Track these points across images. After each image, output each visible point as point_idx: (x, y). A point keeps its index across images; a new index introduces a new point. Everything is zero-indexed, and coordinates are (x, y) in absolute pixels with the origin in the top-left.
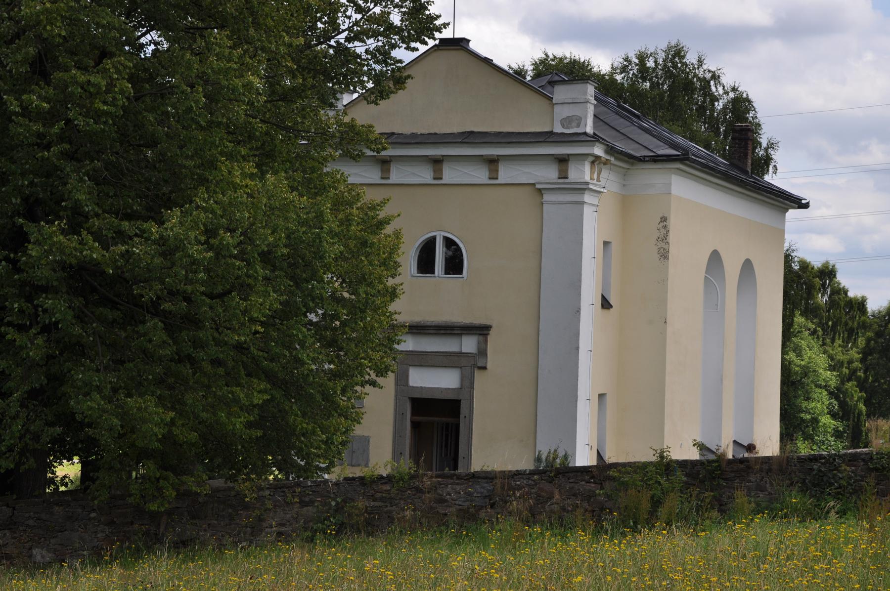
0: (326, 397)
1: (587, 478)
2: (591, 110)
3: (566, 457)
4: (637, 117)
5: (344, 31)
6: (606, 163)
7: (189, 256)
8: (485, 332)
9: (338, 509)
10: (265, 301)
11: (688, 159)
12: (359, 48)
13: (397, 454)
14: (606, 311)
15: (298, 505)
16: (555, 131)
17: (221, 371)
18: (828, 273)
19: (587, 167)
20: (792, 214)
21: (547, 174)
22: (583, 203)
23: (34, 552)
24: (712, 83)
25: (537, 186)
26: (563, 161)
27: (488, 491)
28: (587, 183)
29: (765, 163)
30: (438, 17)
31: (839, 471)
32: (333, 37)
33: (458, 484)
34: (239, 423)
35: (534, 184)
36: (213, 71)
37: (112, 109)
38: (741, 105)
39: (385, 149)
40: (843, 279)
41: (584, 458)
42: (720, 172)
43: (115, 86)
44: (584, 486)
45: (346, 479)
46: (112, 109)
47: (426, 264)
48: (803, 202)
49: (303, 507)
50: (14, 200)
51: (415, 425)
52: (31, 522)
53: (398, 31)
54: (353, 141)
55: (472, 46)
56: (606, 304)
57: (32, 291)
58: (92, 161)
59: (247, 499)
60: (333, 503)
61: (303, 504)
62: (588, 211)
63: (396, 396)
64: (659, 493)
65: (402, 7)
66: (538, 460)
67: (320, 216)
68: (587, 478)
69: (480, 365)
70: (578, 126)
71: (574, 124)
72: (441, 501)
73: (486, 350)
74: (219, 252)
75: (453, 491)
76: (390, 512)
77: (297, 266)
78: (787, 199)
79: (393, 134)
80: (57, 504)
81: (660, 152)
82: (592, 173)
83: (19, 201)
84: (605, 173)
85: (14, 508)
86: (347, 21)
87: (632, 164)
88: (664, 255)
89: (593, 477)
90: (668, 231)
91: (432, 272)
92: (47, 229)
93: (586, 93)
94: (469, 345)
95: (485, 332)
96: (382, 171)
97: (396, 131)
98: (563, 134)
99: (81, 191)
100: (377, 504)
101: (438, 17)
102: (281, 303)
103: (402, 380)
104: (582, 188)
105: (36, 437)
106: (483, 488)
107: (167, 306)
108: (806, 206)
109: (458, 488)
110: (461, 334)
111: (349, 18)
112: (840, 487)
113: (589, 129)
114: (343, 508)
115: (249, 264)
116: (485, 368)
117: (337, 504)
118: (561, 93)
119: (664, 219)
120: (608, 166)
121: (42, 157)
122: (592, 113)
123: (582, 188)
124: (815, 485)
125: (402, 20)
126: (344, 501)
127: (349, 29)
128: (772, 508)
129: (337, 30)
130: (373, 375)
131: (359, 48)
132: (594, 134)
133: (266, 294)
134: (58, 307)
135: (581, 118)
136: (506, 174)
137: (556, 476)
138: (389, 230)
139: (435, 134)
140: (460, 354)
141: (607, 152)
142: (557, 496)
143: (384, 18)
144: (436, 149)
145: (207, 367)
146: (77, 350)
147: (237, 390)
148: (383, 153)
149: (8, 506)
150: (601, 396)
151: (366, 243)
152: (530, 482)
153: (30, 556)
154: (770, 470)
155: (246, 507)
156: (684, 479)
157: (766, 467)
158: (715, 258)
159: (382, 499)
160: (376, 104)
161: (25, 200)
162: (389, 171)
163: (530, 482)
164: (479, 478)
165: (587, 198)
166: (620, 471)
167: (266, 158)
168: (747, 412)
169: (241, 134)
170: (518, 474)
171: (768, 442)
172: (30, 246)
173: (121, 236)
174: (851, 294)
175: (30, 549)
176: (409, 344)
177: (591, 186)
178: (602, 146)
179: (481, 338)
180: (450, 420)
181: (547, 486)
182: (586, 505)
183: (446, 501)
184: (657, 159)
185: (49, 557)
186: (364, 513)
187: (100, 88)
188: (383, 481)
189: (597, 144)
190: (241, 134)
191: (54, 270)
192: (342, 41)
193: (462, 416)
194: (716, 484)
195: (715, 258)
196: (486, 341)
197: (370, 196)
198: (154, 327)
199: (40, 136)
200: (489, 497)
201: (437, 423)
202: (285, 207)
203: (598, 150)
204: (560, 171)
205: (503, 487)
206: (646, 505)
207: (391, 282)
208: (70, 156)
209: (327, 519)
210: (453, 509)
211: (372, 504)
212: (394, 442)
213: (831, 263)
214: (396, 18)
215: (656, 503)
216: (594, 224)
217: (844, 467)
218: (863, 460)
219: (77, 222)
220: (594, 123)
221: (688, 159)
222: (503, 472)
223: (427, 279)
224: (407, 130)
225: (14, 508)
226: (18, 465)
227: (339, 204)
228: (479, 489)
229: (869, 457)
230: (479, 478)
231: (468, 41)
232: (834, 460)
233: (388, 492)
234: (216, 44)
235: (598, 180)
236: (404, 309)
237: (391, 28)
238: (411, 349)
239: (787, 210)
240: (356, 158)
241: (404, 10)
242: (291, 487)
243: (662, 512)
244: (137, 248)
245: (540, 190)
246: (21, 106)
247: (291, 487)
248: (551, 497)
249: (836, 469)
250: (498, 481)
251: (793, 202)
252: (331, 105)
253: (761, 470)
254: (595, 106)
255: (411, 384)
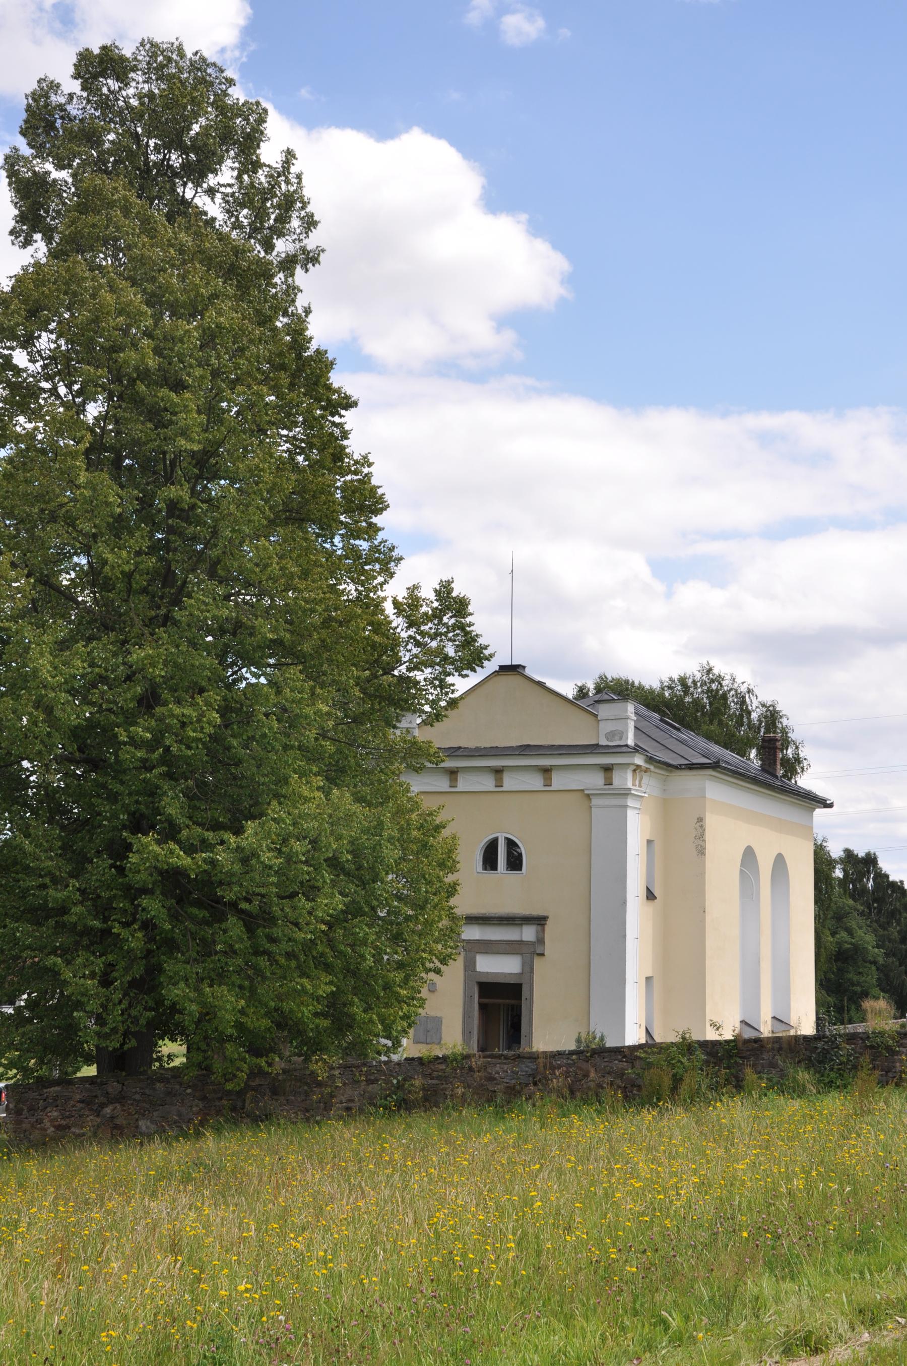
0: (387, 987)
1: (620, 1057)
2: (631, 725)
3: (602, 1038)
4: (678, 730)
5: (405, 662)
6: (647, 771)
7: (262, 863)
8: (543, 922)
9: (400, 1086)
10: (332, 902)
11: (719, 767)
12: (419, 676)
13: (467, 1034)
14: (650, 902)
15: (364, 1083)
16: (601, 743)
17: (293, 964)
18: (870, 860)
19: (629, 775)
20: (819, 812)
21: (596, 780)
22: (626, 806)
23: (140, 1123)
24: (747, 696)
25: (586, 792)
26: (608, 769)
27: (532, 1069)
28: (630, 789)
29: (793, 766)
30: (486, 647)
31: (839, 1049)
32: (396, 668)
33: (505, 1064)
34: (306, 1012)
35: (583, 790)
36: (287, 700)
37: (201, 735)
38: (772, 716)
39: (443, 761)
40: (885, 865)
41: (633, 1036)
42: (749, 777)
43: (205, 716)
44: (617, 1065)
45: (406, 1059)
46: (201, 735)
47: (490, 860)
48: (828, 802)
49: (368, 1085)
50: (122, 817)
51: (482, 1007)
52: (137, 1097)
53: (452, 661)
54: (416, 756)
55: (528, 672)
56: (650, 896)
57: (133, 893)
58: (186, 781)
59: (320, 1078)
60: (395, 1082)
61: (370, 1082)
62: (630, 813)
63: (465, 981)
64: (680, 1071)
65: (455, 641)
66: (579, 1041)
67: (380, 824)
68: (620, 1057)
69: (538, 952)
70: (621, 739)
71: (617, 738)
72: (491, 1079)
73: (543, 938)
74: (290, 859)
75: (502, 1071)
76: (445, 1089)
77: (359, 870)
78: (813, 800)
79: (460, 748)
80: (159, 1081)
81: (695, 761)
82: (634, 780)
83: (126, 817)
84: (645, 780)
85: (123, 1084)
86: (408, 654)
87: (671, 771)
88: (702, 852)
89: (625, 1057)
90: (704, 830)
91: (496, 869)
92: (145, 840)
93: (626, 711)
94: (528, 933)
95: (543, 922)
96: (451, 780)
97: (462, 746)
98: (607, 746)
99: (173, 806)
100: (434, 1082)
101: (486, 647)
102: (344, 905)
103: (470, 965)
104: (625, 793)
105: (135, 1021)
106: (528, 1067)
107: (244, 906)
108: (831, 806)
109: (505, 1067)
110: (522, 924)
111: (410, 651)
112: (841, 1064)
113: (631, 742)
114: (403, 1085)
115: (315, 869)
116: (543, 955)
117: (398, 1082)
118: (604, 711)
119: (700, 820)
120: (648, 774)
121: (145, 778)
122: (633, 728)
123: (625, 793)
124: (820, 1062)
125: (456, 652)
126: (405, 1080)
127: (410, 661)
128: (784, 1086)
129: (399, 661)
130: (438, 964)
131: (419, 676)
132: (636, 745)
133: (332, 896)
134: (154, 907)
135: (623, 733)
136: (559, 781)
137: (591, 1056)
138: (445, 833)
139: (497, 747)
140: (521, 942)
141: (646, 761)
142: (592, 1074)
143: (440, 651)
144: (497, 759)
145: (283, 961)
146: (171, 945)
147: (305, 981)
148: (442, 765)
149: (118, 1082)
150: (648, 979)
151: (426, 847)
152: (570, 1061)
153: (137, 1127)
154: (780, 1049)
155: (320, 1084)
156: (704, 1057)
157: (777, 1046)
158: (749, 855)
159: (438, 1078)
160: (432, 726)
161: (132, 814)
162: (456, 780)
163: (570, 1061)
164: (524, 1057)
165: (630, 802)
166: (645, 1052)
167: (335, 774)
168: (783, 990)
169: (311, 754)
170: (560, 1054)
171: (805, 1023)
172: (131, 855)
173: (206, 845)
174: (891, 879)
175: (137, 1120)
176: (472, 933)
177: (633, 792)
178: (642, 756)
179: (539, 927)
180: (513, 1002)
181: (585, 1065)
182: (618, 1082)
183: (495, 1079)
184: (692, 767)
185: (153, 1127)
186: (426, 1090)
187: (192, 719)
188: (439, 1061)
189: (637, 754)
190: (311, 754)
191: (151, 875)
192: (404, 671)
193: (523, 998)
194: (742, 1063)
195: (749, 855)
196: (543, 931)
197: (428, 804)
198: (234, 927)
199: (144, 761)
200: (533, 1076)
201: (501, 1007)
202: (349, 817)
203: (639, 760)
204: (606, 779)
205: (545, 1066)
206: (667, 1082)
207: (450, 879)
208: (170, 776)
209: (389, 1095)
210: (501, 1087)
211: (430, 1082)
212: (464, 1022)
213: (872, 852)
214: (450, 651)
215: (677, 1081)
216: (638, 826)
217: (843, 1045)
218: (861, 1039)
219: (170, 833)
220: (635, 735)
221: (719, 767)
222: (544, 1053)
223: (491, 875)
224: (472, 744)
225: (123, 1084)
226: (122, 1045)
227: (400, 812)
228: (526, 1067)
229: (865, 1036)
230: (524, 1057)
231: (524, 667)
232: (836, 1039)
233: (443, 1071)
234: (291, 679)
235: (640, 786)
236: (464, 903)
237: (446, 658)
238: (477, 938)
239: (814, 809)
240: (418, 770)
241: (457, 643)
242: (358, 1067)
243: (684, 1089)
244: (220, 856)
245: (588, 796)
246: (128, 737)
247: (358, 1067)
248: (586, 1075)
249: (837, 1047)
250: (540, 1060)
251: (819, 802)
252: (395, 727)
253: (773, 1049)
254: (635, 721)
255: (478, 969)
